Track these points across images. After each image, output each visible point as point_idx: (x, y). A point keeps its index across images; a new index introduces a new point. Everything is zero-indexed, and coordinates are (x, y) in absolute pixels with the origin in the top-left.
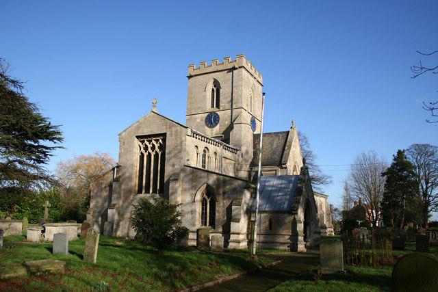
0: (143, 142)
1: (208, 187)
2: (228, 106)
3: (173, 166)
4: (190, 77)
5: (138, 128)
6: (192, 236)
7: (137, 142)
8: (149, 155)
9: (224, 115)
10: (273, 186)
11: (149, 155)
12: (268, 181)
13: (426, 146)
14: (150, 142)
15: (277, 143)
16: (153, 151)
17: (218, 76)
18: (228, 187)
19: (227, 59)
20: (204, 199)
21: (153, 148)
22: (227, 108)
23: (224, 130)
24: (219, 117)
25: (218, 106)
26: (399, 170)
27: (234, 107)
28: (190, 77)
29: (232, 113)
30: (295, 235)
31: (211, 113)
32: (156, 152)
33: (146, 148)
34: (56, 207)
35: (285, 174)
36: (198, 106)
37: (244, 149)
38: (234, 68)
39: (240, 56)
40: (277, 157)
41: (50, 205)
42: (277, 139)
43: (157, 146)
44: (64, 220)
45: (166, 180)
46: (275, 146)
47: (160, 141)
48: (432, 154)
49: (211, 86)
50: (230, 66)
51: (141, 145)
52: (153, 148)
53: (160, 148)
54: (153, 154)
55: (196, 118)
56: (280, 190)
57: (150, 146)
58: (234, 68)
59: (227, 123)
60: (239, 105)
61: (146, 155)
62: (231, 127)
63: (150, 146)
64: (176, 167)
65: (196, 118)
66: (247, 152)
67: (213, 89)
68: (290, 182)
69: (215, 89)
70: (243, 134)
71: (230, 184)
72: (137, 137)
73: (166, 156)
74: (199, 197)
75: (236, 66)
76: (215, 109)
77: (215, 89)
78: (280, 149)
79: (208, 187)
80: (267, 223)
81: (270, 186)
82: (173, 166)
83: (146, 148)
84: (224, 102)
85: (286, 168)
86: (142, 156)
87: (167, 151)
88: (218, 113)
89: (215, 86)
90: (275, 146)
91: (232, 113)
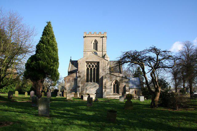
0: (88, 64)
2: (101, 50)
4: (84, 37)
5: (87, 59)
7: (86, 64)
8: (91, 69)
11: (91, 69)
14: (91, 64)
21: (93, 66)
22: (100, 51)
28: (84, 37)
33: (90, 66)
36: (89, 49)
38: (103, 37)
39: (105, 33)
44: (100, 98)
45: (100, 77)
50: (102, 36)
52: (93, 66)
53: (96, 66)
55: (88, 53)
57: (91, 66)
58: (103, 37)
60: (105, 51)
63: (91, 66)
65: (88, 53)
67: (94, 43)
69: (95, 43)
72: (86, 62)
74: (113, 84)
75: (86, 36)
76: (96, 51)
77: (95, 43)
83: (90, 66)
84: (99, 48)
86: (88, 69)
89: (95, 42)
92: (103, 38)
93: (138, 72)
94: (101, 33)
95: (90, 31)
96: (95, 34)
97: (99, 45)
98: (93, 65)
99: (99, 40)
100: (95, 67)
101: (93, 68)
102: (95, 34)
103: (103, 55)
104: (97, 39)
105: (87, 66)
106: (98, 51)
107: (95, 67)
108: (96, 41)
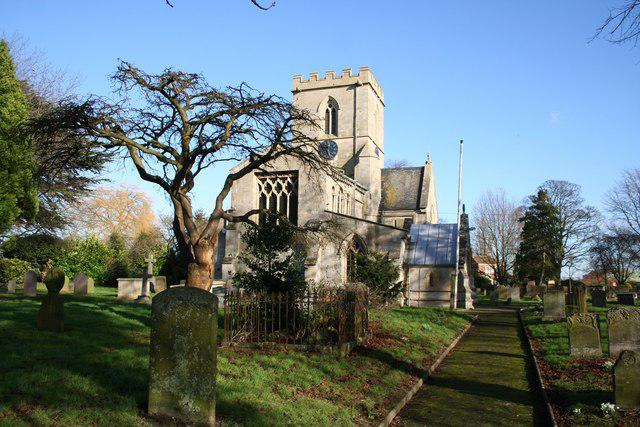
0: (263, 180)
1: (356, 237)
3: (309, 211)
6: (221, 298)
9: (344, 146)
10: (428, 236)
12: (422, 230)
13: (563, 183)
14: (274, 180)
15: (411, 181)
16: (268, 193)
17: (336, 94)
18: (381, 237)
19: (347, 71)
20: (351, 251)
21: (279, 188)
23: (346, 161)
24: (337, 147)
25: (335, 132)
26: (539, 216)
27: (357, 135)
29: (354, 143)
30: (462, 291)
31: (326, 141)
32: (283, 194)
33: (269, 188)
34: (100, 261)
35: (423, 220)
37: (372, 189)
38: (357, 85)
39: (364, 69)
40: (412, 200)
41: (155, 260)
42: (408, 177)
43: (284, 185)
46: (407, 185)
47: (289, 180)
48: (571, 193)
49: (325, 106)
50: (353, 81)
51: (261, 183)
52: (279, 188)
53: (289, 187)
54: (279, 196)
56: (438, 241)
57: (274, 186)
58: (357, 85)
59: (349, 154)
60: (364, 133)
61: (268, 196)
62: (355, 159)
63: (274, 186)
64: (313, 212)
66: (376, 193)
67: (327, 111)
68: (448, 231)
69: (330, 110)
70: (371, 169)
71: (385, 234)
73: (299, 199)
75: (361, 83)
76: (331, 136)
77: (330, 110)
78: (414, 193)
79: (356, 237)
80: (428, 278)
81: (425, 236)
82: (309, 211)
83: (269, 188)
84: (344, 127)
85: (425, 213)
86: (263, 198)
87: (300, 192)
88: (336, 141)
89: (330, 106)
90: (407, 185)
91: (354, 143)
92: (358, 89)
93: (537, 207)
94: (347, 71)
95: (228, 85)
96: (329, 79)
97: (344, 114)
98: (268, 184)
99: (343, 97)
100: (286, 192)
101: (268, 193)
102: (329, 79)
103: (357, 149)
104: (336, 94)
105: (260, 189)
106: (340, 136)
107: (286, 192)
108: (332, 103)
